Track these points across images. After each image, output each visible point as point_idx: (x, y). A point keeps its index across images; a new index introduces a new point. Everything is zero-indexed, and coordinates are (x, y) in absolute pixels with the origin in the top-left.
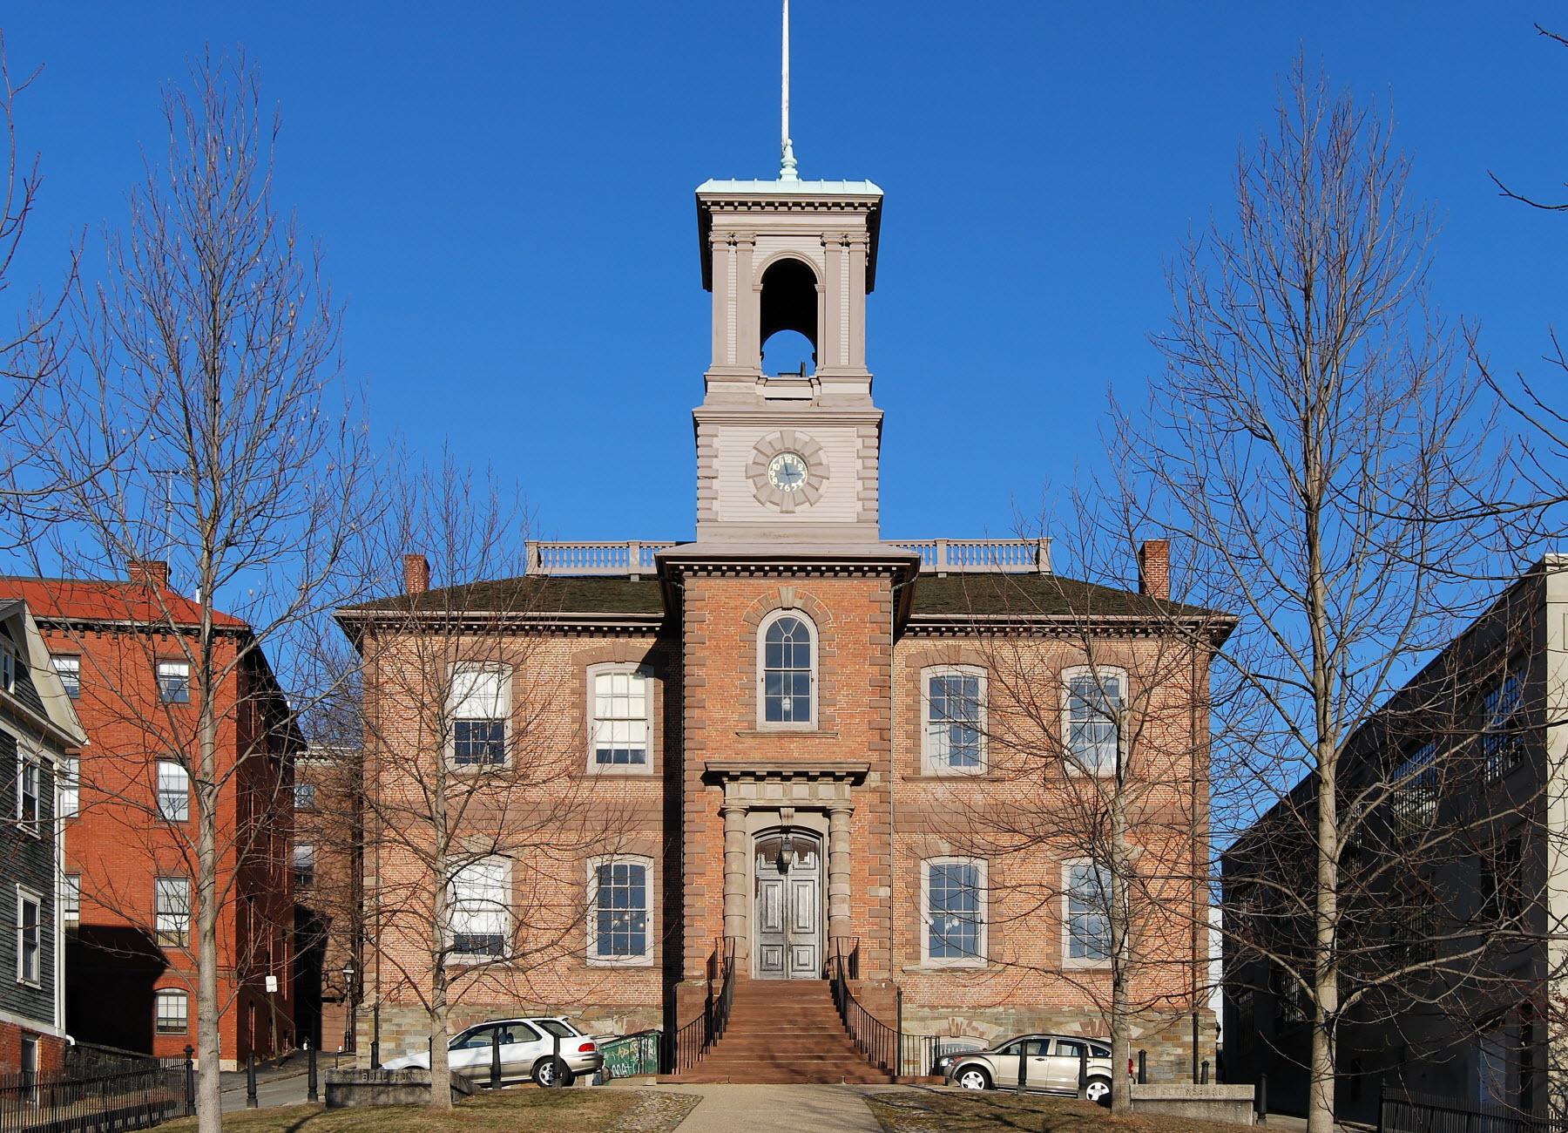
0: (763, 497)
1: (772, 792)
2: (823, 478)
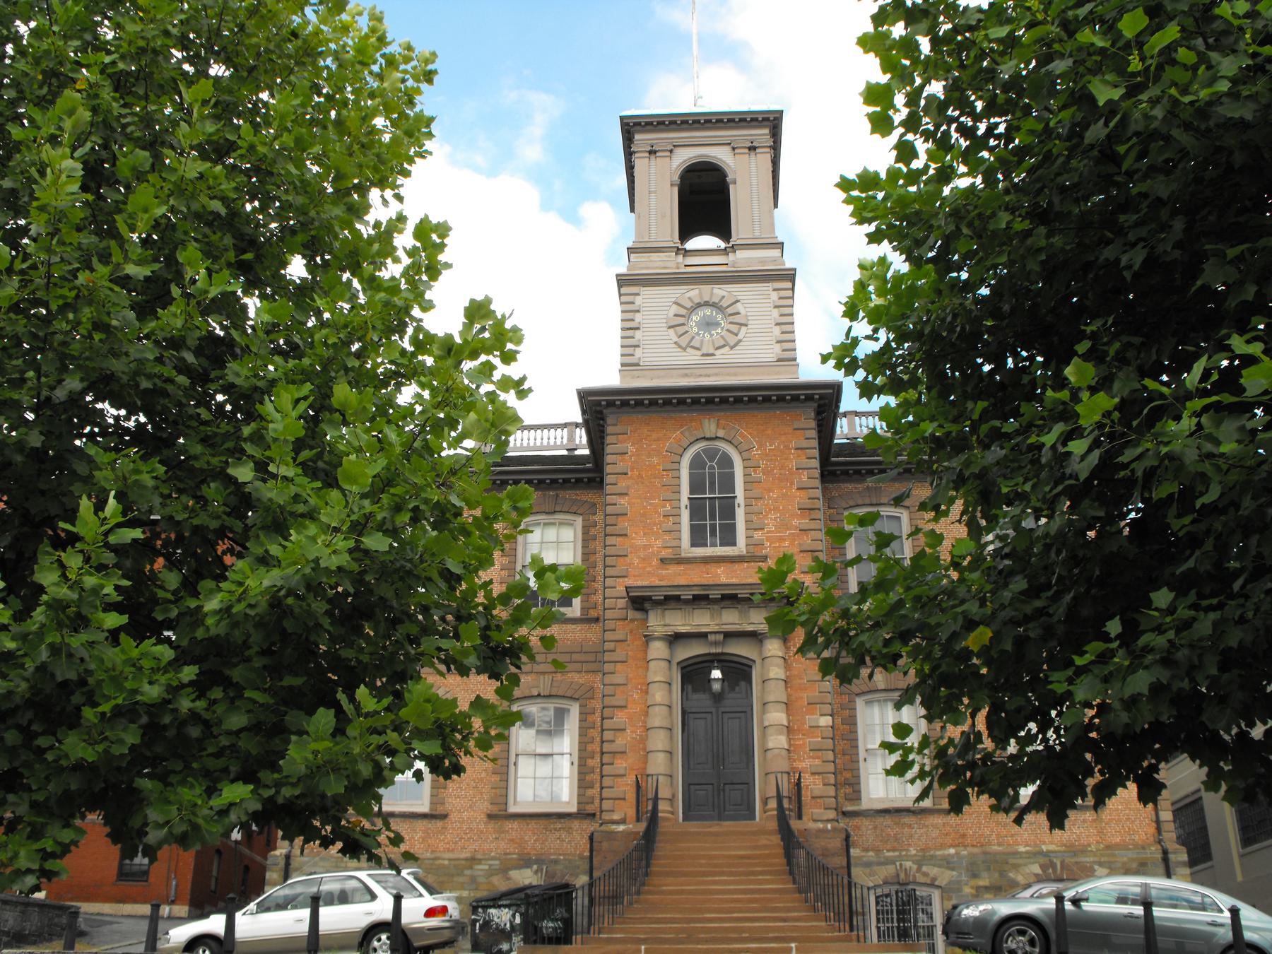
1: (701, 620)
2: (742, 325)
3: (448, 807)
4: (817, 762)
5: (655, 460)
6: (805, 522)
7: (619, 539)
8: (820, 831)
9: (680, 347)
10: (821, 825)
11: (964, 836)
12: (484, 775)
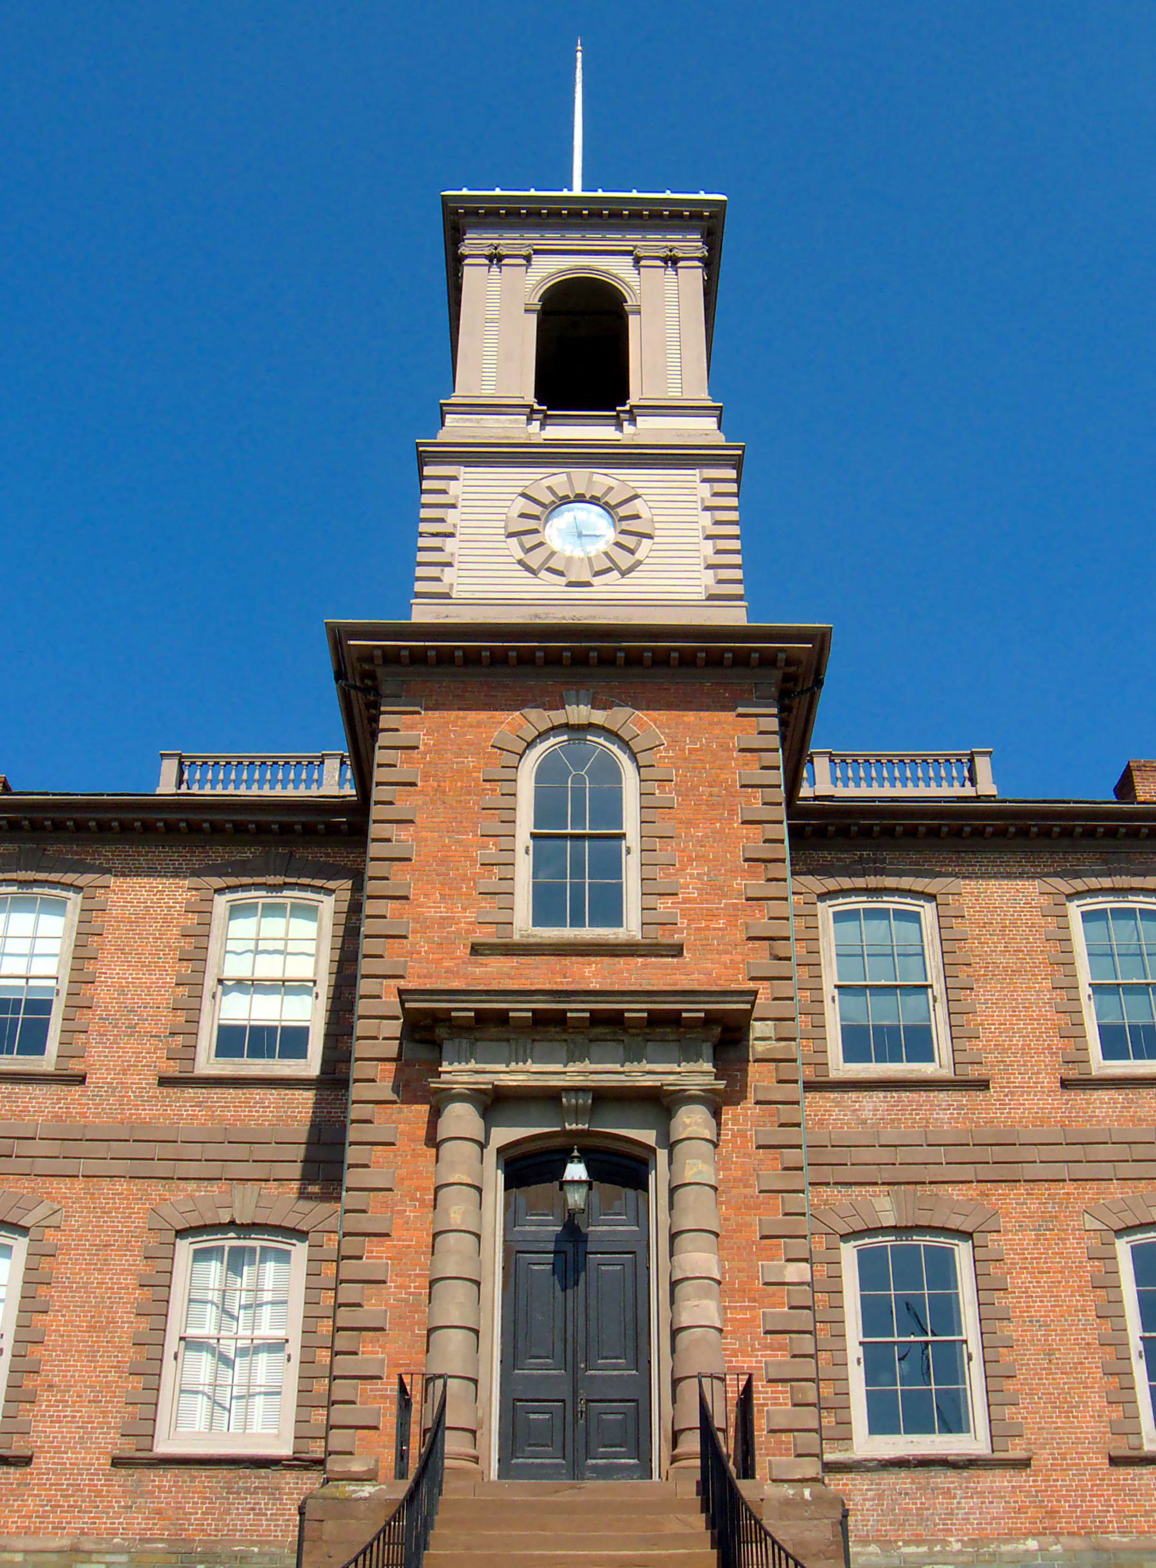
0: (534, 560)
3: (36, 1439)
4: (781, 1357)
5: (471, 762)
6: (757, 885)
7: (391, 904)
8: (787, 1502)
9: (528, 569)
10: (789, 1491)
11: (1052, 1513)
12: (114, 1375)
